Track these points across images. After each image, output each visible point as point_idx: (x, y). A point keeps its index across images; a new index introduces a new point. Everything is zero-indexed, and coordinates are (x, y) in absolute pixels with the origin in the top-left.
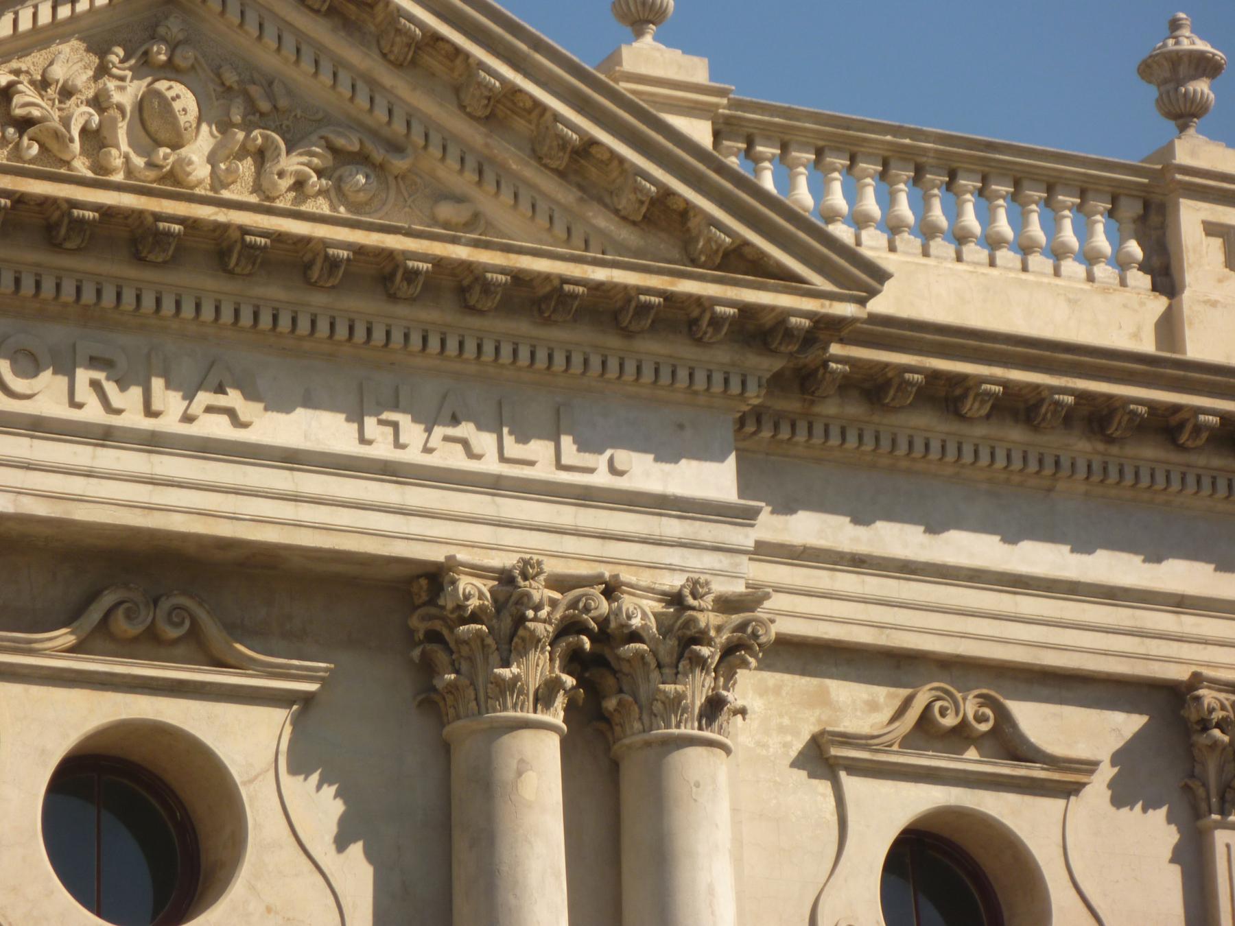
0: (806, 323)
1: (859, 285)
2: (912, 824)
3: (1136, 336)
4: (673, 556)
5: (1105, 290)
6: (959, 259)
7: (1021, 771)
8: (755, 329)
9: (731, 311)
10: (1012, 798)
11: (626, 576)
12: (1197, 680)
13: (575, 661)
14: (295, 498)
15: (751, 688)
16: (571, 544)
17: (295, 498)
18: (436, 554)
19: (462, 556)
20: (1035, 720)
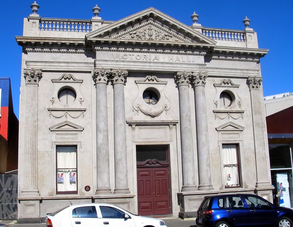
0: (210, 47)
1: (214, 43)
2: (224, 91)
3: (243, 46)
4: (183, 69)
5: (239, 42)
6: (219, 40)
7: (233, 86)
8: (205, 48)
9: (51, 43)
10: (232, 88)
11: (194, 71)
12: (249, 77)
13: (190, 79)
14: (163, 67)
15: (208, 79)
16: (189, 69)
17: (163, 67)
18: (176, 71)
19: (178, 70)
20: (234, 81)
